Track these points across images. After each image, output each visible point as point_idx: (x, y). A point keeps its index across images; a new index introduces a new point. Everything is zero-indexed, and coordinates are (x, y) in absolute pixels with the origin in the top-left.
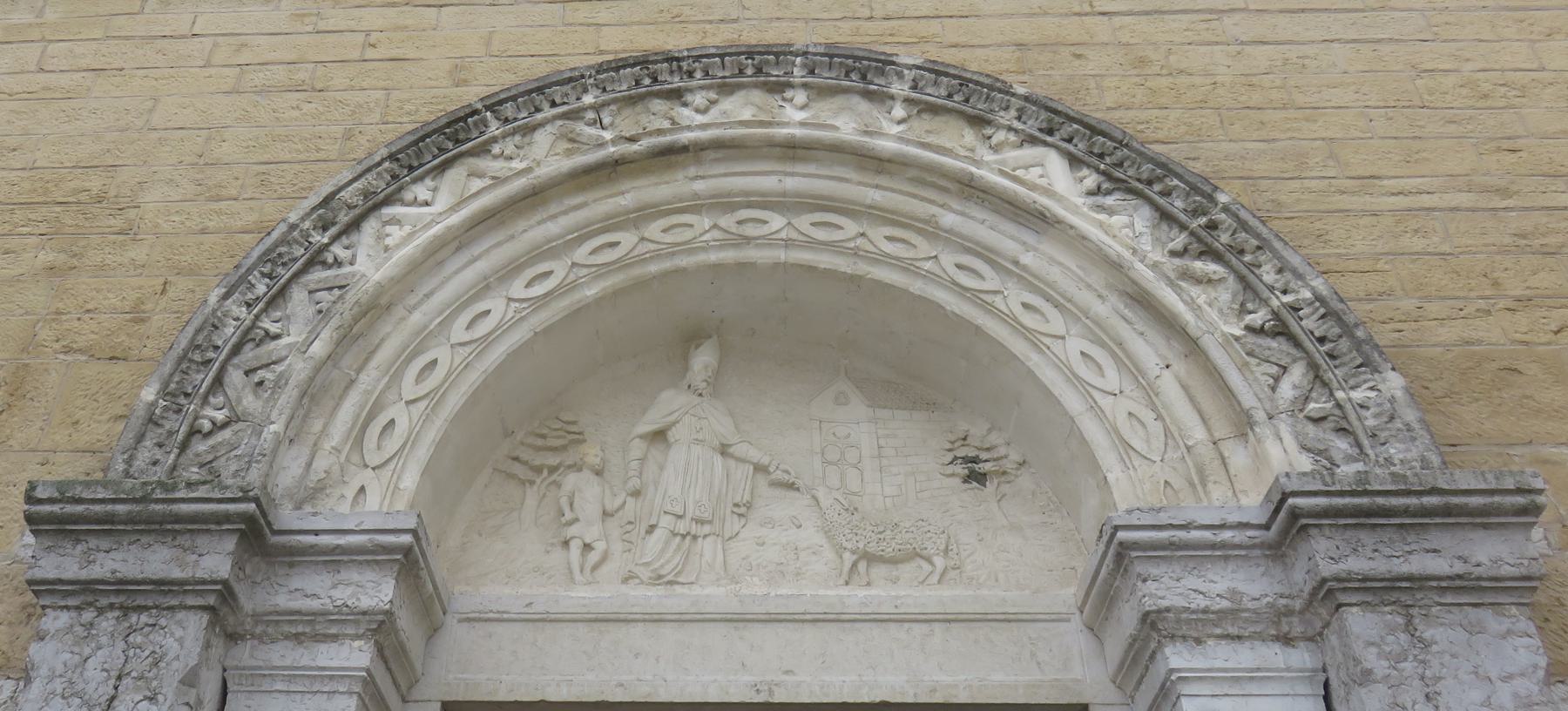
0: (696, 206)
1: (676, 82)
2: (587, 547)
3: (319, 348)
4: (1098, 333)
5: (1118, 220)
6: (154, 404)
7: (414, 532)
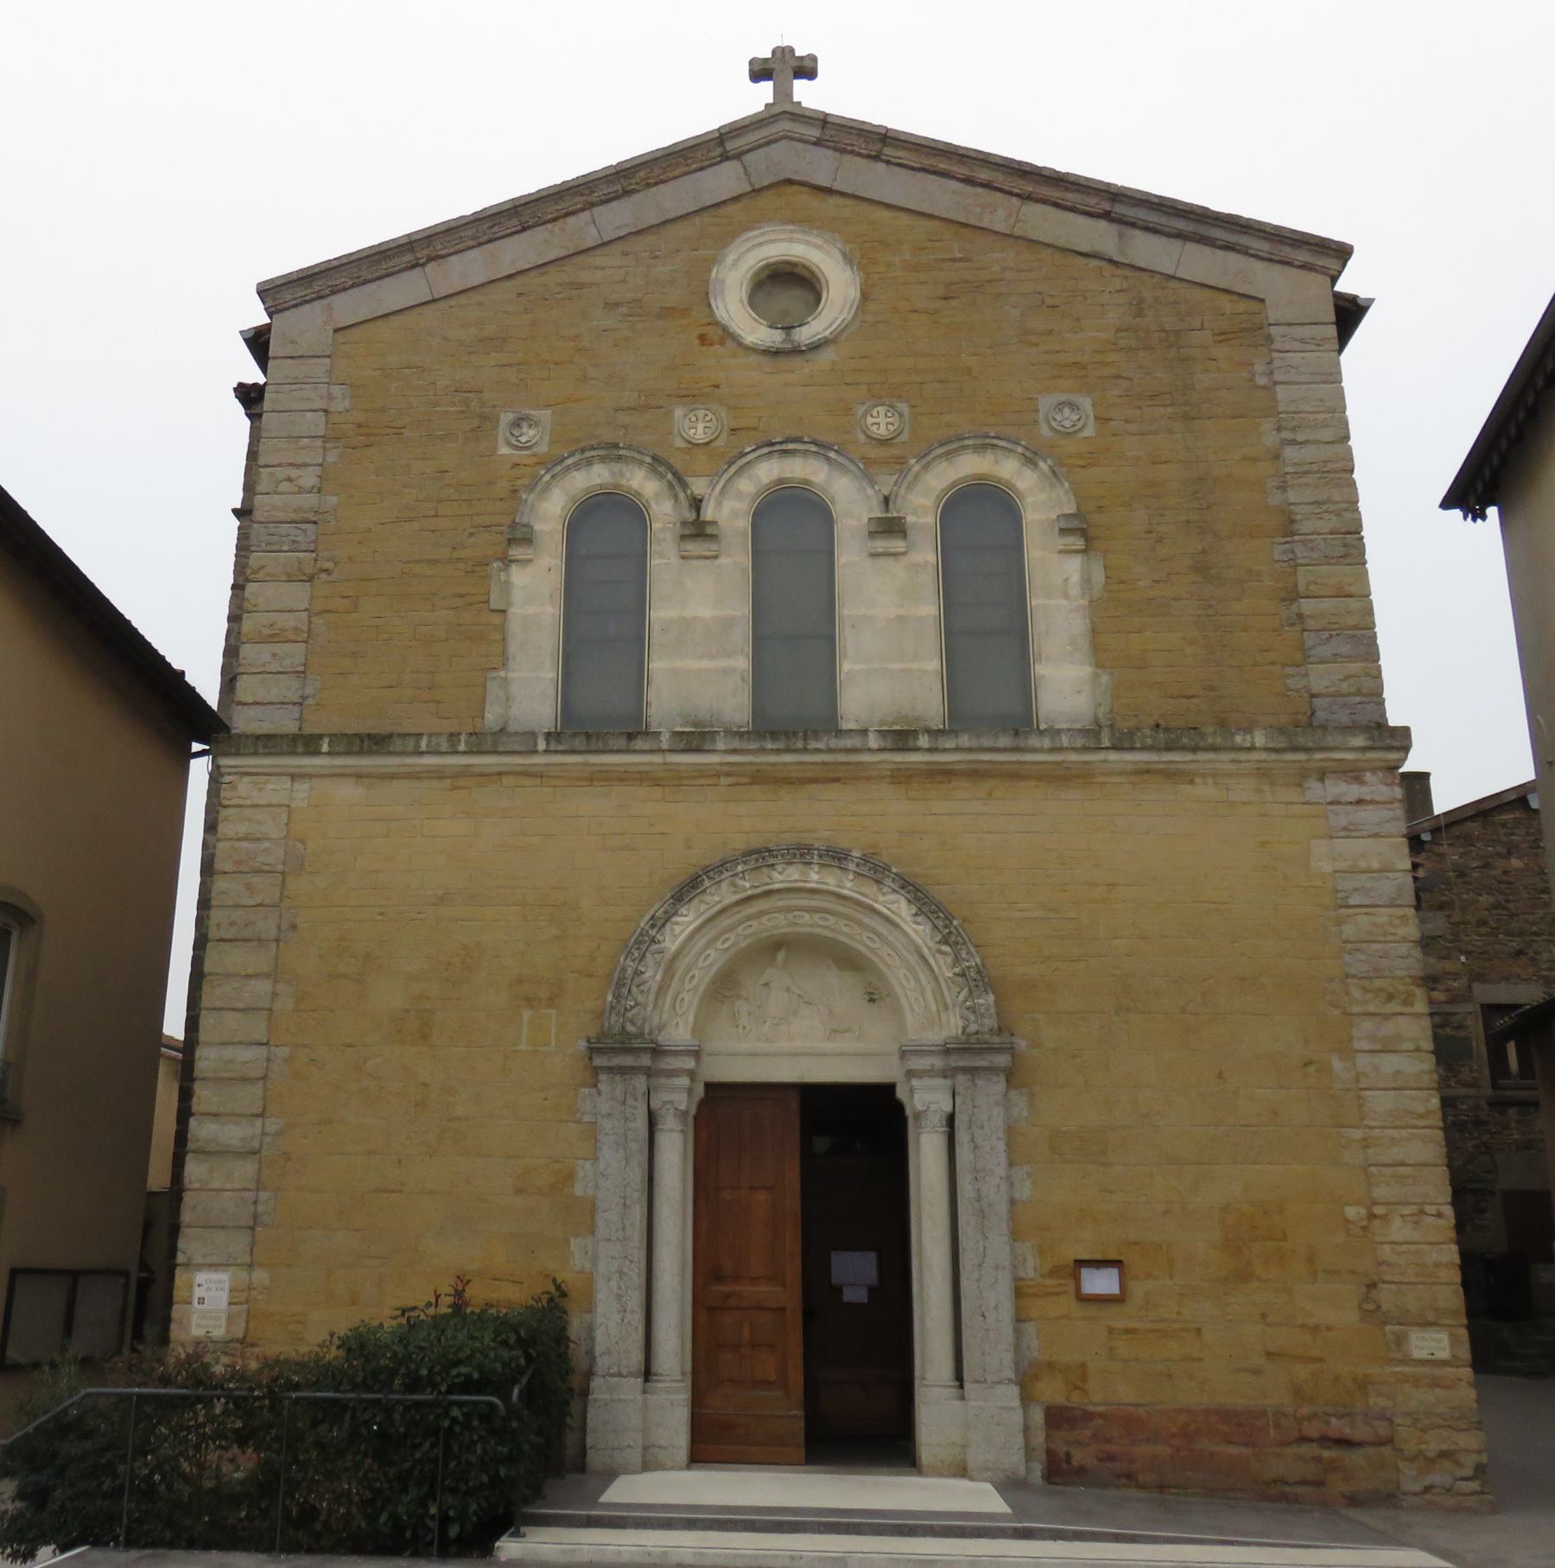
0: (780, 910)
1: (772, 861)
2: (744, 1027)
3: (658, 977)
4: (910, 969)
5: (921, 928)
6: (612, 1002)
7: (699, 1046)
